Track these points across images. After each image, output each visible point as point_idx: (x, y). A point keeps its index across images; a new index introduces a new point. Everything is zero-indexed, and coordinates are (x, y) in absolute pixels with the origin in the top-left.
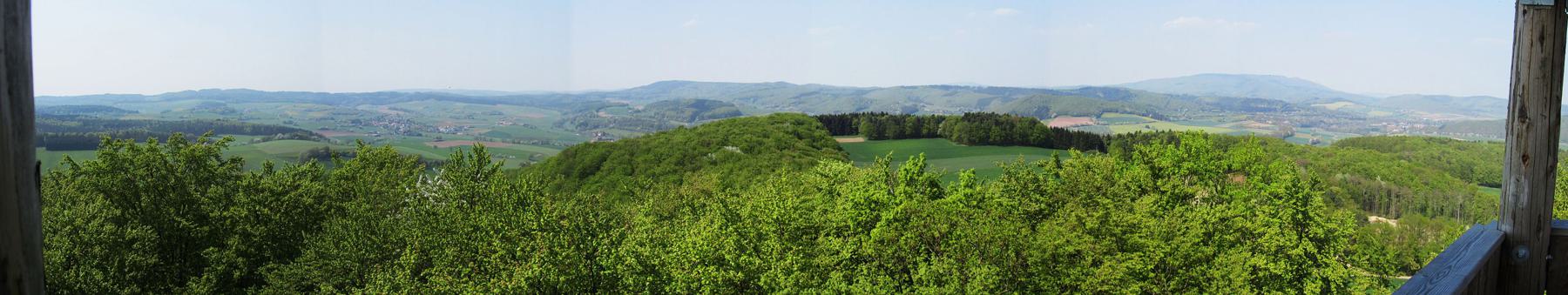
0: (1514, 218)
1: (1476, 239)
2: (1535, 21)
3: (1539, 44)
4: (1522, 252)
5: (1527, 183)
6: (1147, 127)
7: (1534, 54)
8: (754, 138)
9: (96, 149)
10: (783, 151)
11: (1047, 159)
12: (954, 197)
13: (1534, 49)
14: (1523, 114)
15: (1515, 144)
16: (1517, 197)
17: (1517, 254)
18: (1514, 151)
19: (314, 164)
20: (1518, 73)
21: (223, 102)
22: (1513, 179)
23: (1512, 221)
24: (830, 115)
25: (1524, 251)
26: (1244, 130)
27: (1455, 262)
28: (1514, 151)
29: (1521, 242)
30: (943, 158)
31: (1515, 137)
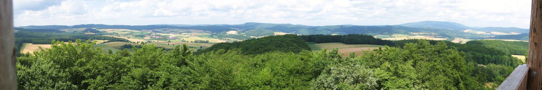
0: (532, 62)
1: (521, 69)
2: (538, 2)
3: (540, 9)
4: (535, 73)
5: (536, 51)
6: (407, 38)
7: (538, 13)
8: (279, 42)
9: (50, 44)
10: (289, 47)
11: (377, 47)
12: (451, 66)
13: (538, 11)
14: (535, 30)
15: (532, 40)
16: (533, 57)
17: (533, 74)
18: (532, 42)
19: (450, 82)
20: (533, 18)
21: (95, 29)
22: (532, 51)
23: (531, 64)
24: (305, 35)
25: (535, 73)
26: (59, 34)
27: (516, 76)
28: (532, 42)
29: (534, 70)
30: (520, 55)
31: (532, 38)
